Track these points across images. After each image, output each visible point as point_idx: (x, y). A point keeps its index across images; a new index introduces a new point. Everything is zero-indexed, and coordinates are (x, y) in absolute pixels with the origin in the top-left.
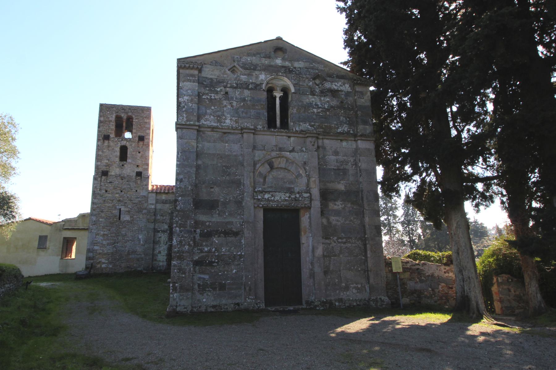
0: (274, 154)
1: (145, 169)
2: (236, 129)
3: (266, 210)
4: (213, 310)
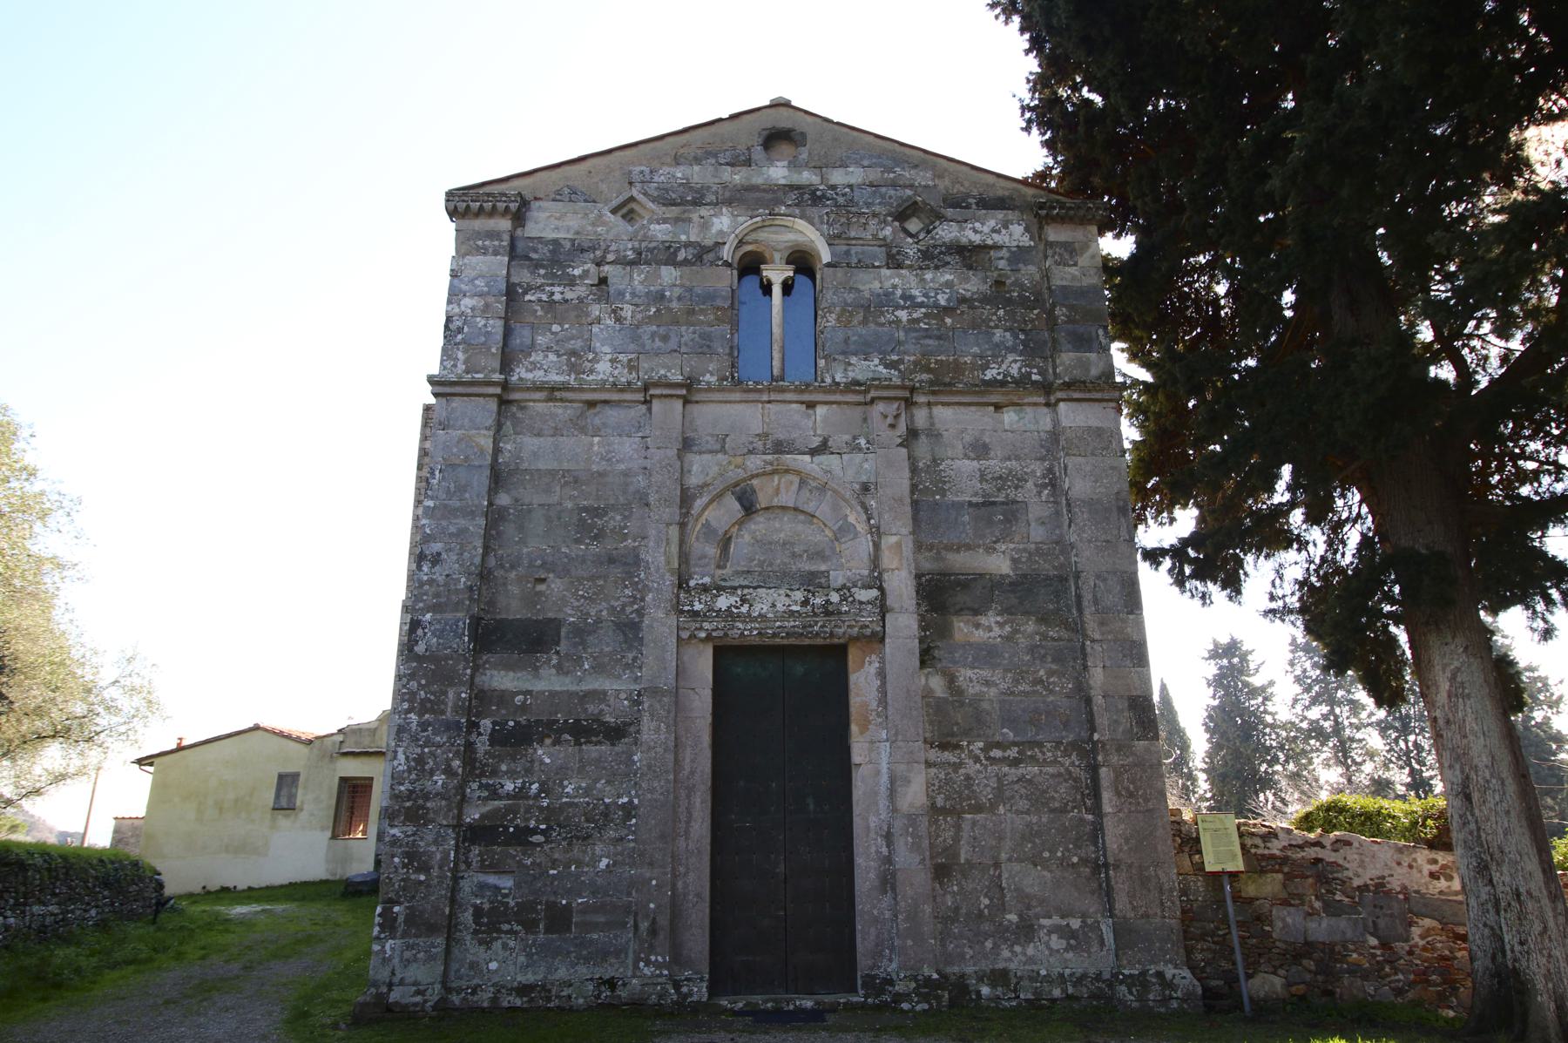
0: (755, 463)
2: (629, 387)
4: (518, 1002)
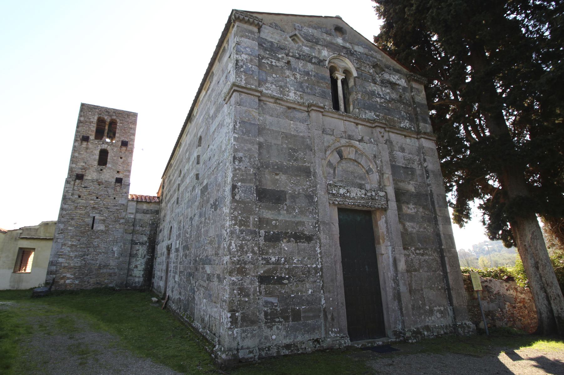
0: (343, 141)
1: (126, 175)
2: (302, 104)
3: (341, 211)
4: (287, 352)
